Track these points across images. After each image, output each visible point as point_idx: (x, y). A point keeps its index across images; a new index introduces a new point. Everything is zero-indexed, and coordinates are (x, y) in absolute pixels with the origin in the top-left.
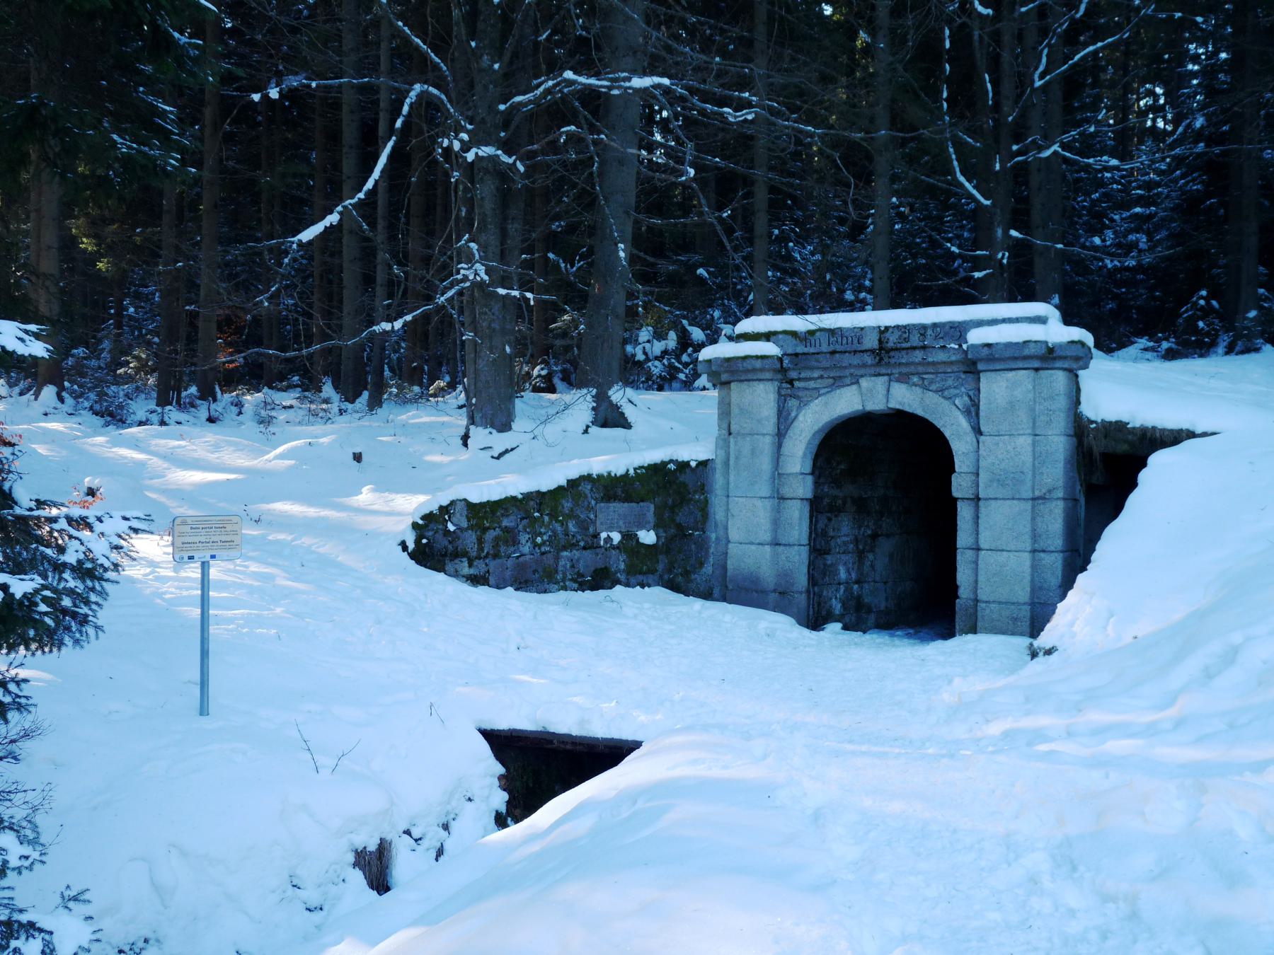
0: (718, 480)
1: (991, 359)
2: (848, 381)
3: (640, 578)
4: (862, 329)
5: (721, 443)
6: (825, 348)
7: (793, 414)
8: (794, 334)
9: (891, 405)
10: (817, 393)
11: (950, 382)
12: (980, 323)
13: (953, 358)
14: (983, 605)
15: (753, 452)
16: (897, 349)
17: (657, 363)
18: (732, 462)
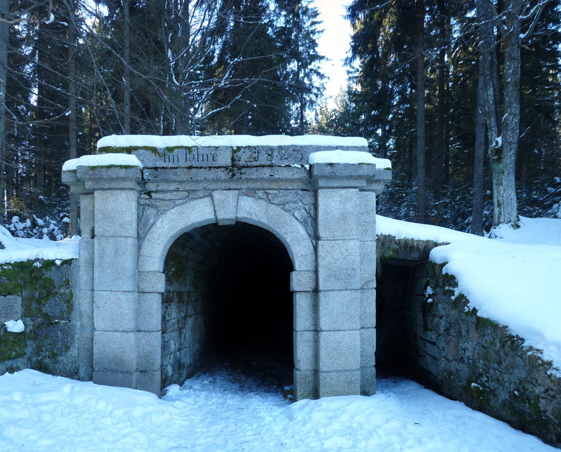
0: (82, 277)
1: (331, 177)
2: (201, 194)
3: (9, 363)
4: (217, 148)
5: (84, 244)
6: (182, 163)
7: (152, 221)
8: (154, 150)
9: (239, 216)
10: (173, 203)
11: (290, 198)
12: (318, 148)
13: (296, 176)
14: (325, 375)
15: (116, 251)
16: (248, 167)
17: (21, 232)
18: (96, 261)
